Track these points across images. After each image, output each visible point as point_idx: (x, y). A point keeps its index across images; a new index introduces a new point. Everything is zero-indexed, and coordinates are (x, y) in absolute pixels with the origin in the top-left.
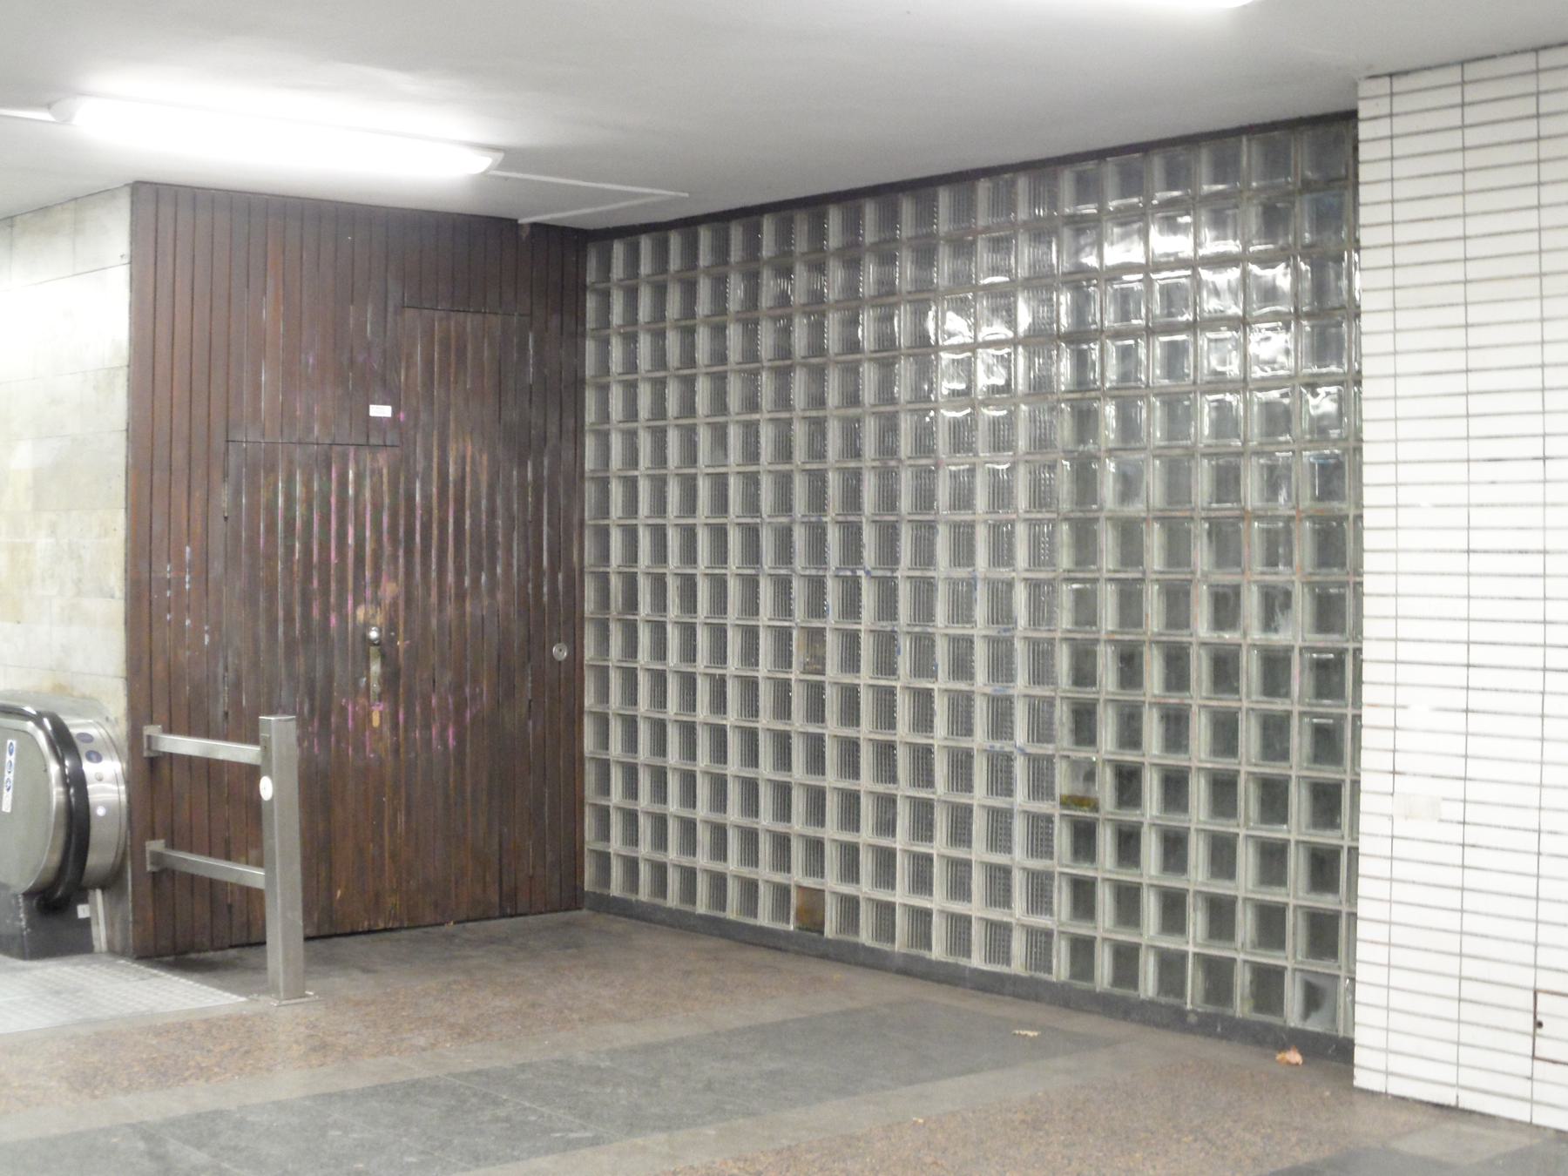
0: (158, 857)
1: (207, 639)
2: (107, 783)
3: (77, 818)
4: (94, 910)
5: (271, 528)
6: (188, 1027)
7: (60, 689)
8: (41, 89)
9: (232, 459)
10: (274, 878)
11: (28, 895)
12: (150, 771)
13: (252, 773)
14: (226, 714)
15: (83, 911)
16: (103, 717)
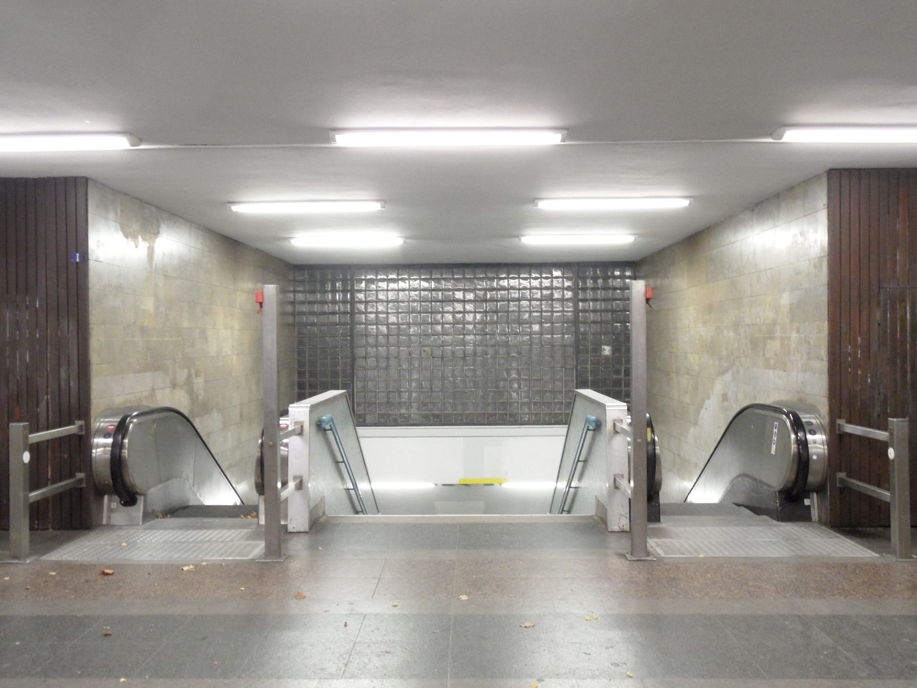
0: (842, 480)
1: (869, 380)
2: (818, 442)
3: (802, 460)
4: (812, 502)
5: (903, 329)
6: (845, 566)
7: (801, 400)
8: (775, 127)
9: (882, 298)
10: (895, 496)
11: (779, 492)
12: (838, 440)
13: (885, 446)
14: (879, 415)
15: (807, 502)
16: (818, 414)
